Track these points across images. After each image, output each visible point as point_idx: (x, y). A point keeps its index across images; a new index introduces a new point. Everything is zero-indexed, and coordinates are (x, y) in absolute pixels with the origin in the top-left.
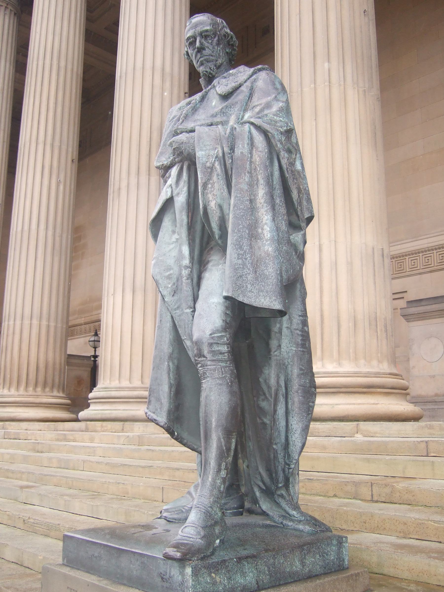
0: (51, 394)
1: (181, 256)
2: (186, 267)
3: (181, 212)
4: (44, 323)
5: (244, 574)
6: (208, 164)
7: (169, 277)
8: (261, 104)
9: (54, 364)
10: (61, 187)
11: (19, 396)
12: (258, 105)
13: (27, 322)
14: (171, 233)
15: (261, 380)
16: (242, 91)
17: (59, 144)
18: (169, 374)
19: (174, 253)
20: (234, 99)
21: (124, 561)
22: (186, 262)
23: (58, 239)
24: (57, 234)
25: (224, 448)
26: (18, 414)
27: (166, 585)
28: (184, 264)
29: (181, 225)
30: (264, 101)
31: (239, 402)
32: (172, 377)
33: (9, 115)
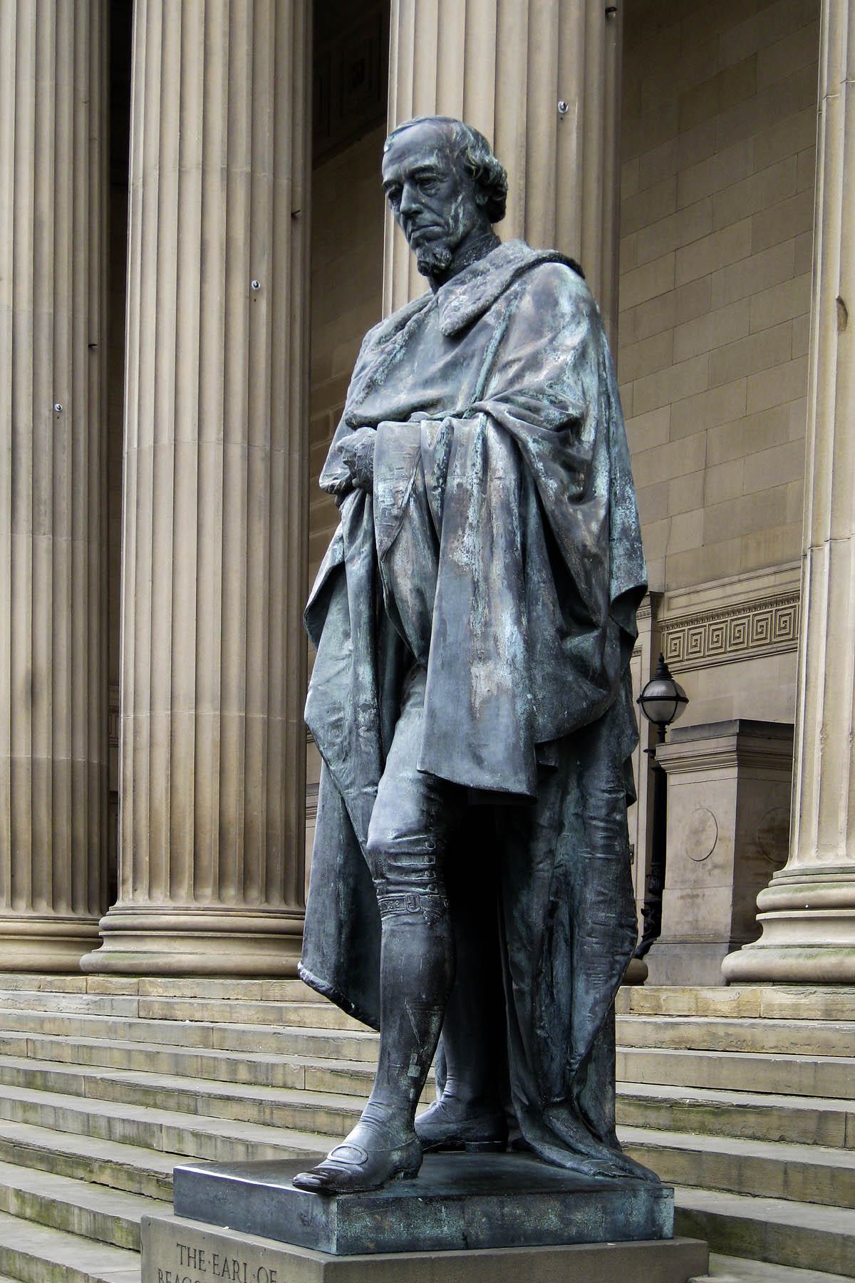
0: (265, 906)
1: (357, 686)
2: (366, 707)
3: (357, 596)
4: (234, 713)
5: (438, 1221)
6: (395, 512)
7: (337, 725)
8: (519, 360)
9: (269, 824)
10: (263, 306)
11: (178, 911)
12: (514, 361)
13: (185, 713)
14: (341, 635)
15: (516, 914)
16: (486, 325)
17: (249, 169)
18: (337, 904)
19: (347, 679)
20: (467, 345)
21: (257, 1202)
22: (367, 696)
23: (260, 468)
24: (259, 455)
25: (415, 1031)
26: (178, 957)
27: (309, 1229)
28: (362, 702)
29: (358, 625)
30: (528, 350)
31: (447, 954)
32: (342, 908)
33: (101, 11)
